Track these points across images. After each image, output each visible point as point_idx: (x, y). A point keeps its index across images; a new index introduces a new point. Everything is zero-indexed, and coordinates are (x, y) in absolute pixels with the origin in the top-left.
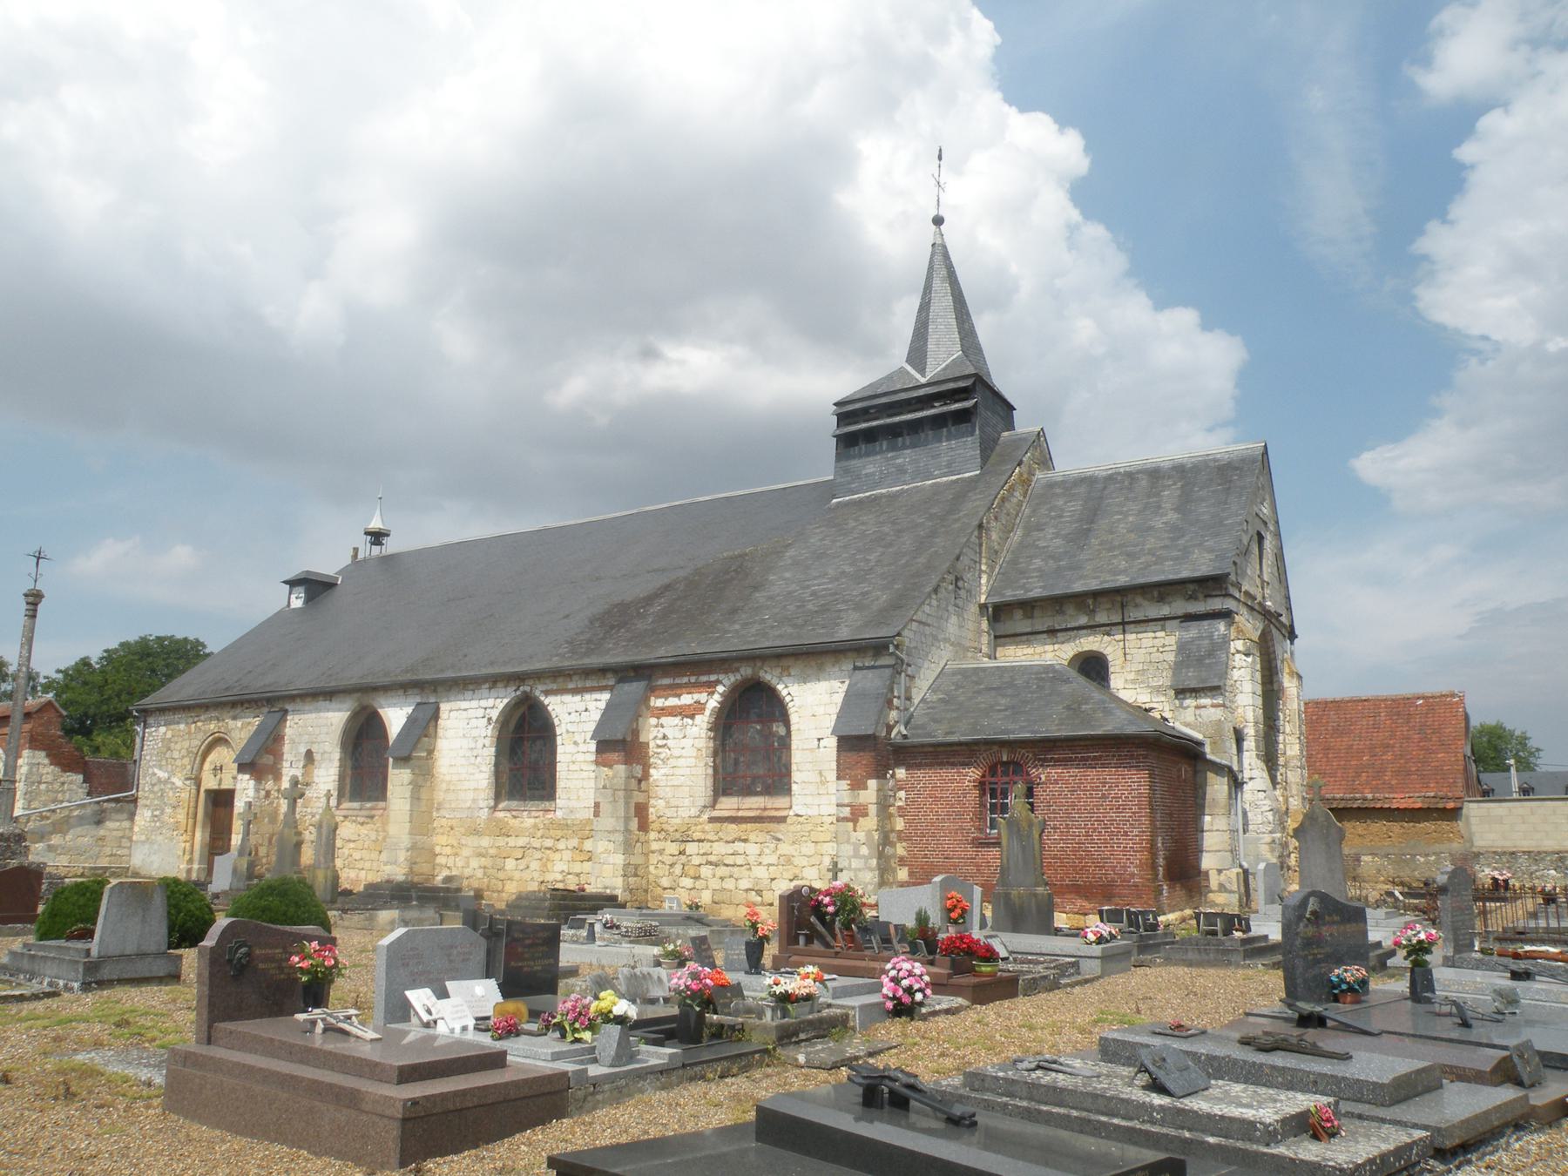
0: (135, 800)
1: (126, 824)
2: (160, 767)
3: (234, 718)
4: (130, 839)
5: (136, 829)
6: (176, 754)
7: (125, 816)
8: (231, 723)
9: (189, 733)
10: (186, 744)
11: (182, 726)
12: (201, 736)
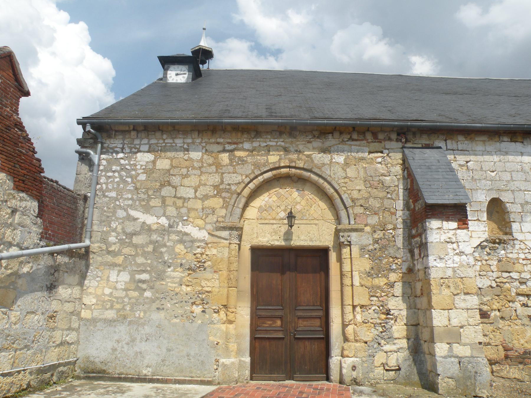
0: (85, 255)
1: (76, 291)
2: (147, 209)
3: (325, 151)
4: (78, 314)
5: (89, 300)
6: (187, 192)
7: (77, 278)
8: (319, 158)
9: (218, 165)
10: (215, 179)
11: (195, 155)
12: (248, 169)
